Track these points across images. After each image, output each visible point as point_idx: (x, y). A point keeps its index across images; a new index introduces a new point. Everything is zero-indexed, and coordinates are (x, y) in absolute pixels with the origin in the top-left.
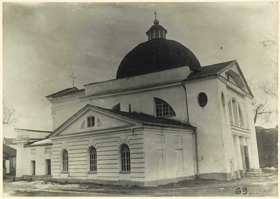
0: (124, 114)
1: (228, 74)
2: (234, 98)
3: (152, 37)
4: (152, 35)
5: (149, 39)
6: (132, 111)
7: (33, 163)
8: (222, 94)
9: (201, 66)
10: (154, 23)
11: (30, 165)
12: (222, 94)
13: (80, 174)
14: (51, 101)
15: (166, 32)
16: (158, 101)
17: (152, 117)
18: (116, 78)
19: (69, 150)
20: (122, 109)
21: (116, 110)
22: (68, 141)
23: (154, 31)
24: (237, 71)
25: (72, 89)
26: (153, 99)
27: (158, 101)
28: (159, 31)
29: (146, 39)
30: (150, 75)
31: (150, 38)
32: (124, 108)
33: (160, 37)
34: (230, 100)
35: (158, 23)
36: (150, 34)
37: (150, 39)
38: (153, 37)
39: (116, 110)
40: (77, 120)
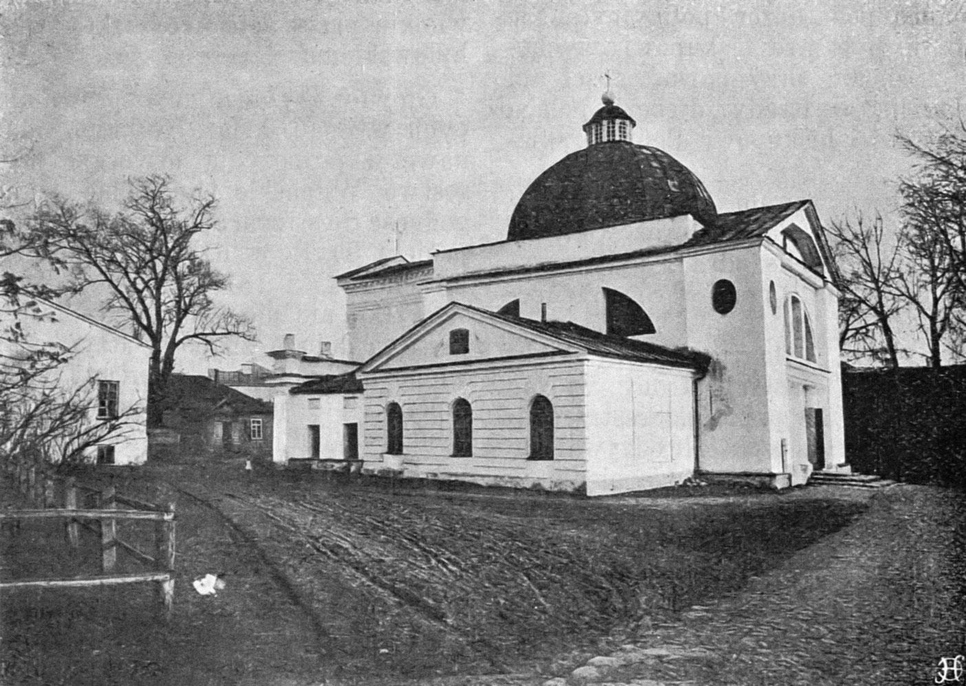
0: (530, 324)
1: (786, 233)
2: (797, 293)
3: (597, 138)
4: (599, 135)
5: (590, 141)
6: (549, 318)
7: (311, 432)
8: (772, 284)
9: (719, 212)
10: (605, 103)
11: (306, 436)
12: (772, 284)
13: (501, 412)
14: (346, 287)
15: (633, 124)
16: (612, 296)
17: (596, 336)
18: (505, 238)
19: (405, 404)
20: (524, 313)
21: (511, 312)
22: (401, 384)
23: (605, 122)
24: (649, 341)
25: (393, 261)
26: (601, 290)
27: (612, 296)
28: (618, 121)
29: (580, 142)
30: (597, 234)
31: (594, 138)
32: (529, 311)
33: (617, 138)
34: (787, 300)
35: (612, 103)
36: (594, 131)
37: (594, 143)
38: (601, 138)
39: (511, 312)
40: (559, 264)
